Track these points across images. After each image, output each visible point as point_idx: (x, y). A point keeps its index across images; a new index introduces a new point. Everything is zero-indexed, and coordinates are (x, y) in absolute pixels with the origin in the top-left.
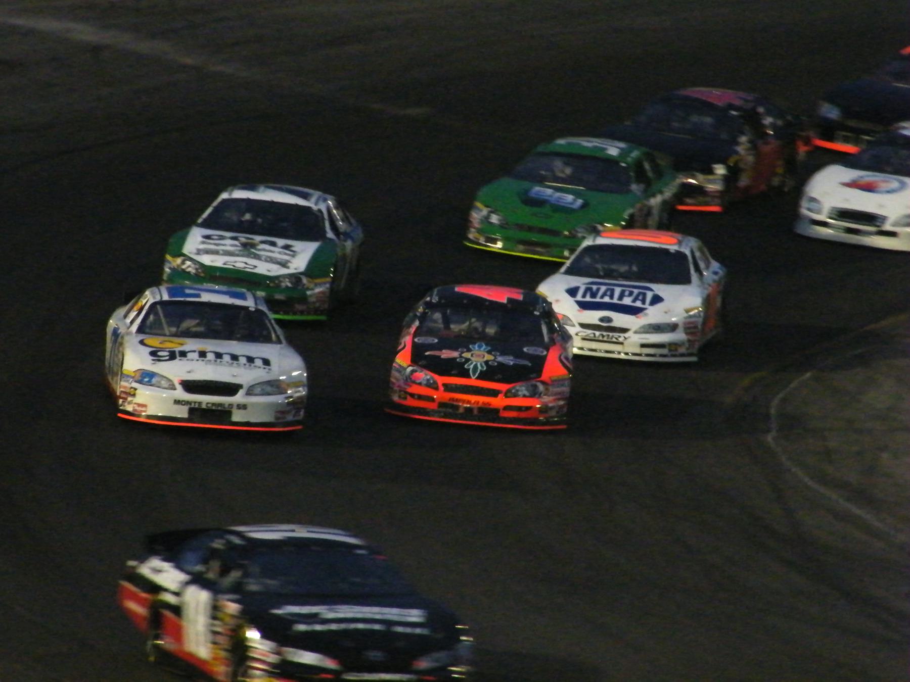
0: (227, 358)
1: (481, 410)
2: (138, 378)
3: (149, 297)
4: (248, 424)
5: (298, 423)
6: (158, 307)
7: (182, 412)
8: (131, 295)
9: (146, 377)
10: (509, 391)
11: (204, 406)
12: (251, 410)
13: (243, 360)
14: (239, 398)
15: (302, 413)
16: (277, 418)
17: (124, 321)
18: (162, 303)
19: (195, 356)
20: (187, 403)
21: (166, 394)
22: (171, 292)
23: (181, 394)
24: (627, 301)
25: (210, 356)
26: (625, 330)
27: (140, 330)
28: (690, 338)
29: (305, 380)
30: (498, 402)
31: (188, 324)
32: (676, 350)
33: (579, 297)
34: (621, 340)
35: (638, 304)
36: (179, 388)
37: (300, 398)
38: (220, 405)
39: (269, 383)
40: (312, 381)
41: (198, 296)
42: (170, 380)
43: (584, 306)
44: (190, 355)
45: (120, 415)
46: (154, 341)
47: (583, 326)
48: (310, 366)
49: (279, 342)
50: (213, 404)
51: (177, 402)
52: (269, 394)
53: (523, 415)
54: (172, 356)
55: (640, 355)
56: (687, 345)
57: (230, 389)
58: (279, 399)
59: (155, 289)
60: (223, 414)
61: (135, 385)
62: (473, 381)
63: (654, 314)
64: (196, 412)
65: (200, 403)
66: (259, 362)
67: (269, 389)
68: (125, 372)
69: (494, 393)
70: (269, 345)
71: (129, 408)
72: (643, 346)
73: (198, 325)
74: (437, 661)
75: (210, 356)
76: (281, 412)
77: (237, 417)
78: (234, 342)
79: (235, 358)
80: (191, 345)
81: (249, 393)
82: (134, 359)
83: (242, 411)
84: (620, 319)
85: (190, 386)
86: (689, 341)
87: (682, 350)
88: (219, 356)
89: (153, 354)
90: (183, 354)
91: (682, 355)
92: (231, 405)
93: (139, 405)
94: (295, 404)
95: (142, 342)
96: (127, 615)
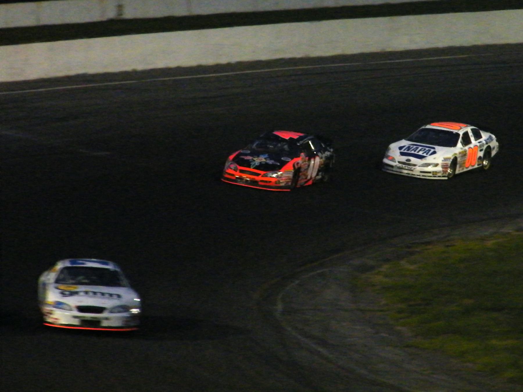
1: (251, 181)
3: (60, 266)
5: (135, 327)
7: (76, 322)
8: (50, 266)
9: (58, 305)
10: (264, 174)
12: (112, 320)
17: (49, 277)
21: (68, 313)
24: (421, 153)
26: (415, 165)
27: (57, 281)
28: (444, 169)
31: (81, 278)
32: (436, 174)
33: (402, 151)
34: (412, 169)
35: (425, 155)
38: (96, 318)
43: (402, 154)
46: (62, 287)
47: (399, 162)
48: (141, 295)
54: (72, 294)
55: (419, 175)
56: (442, 172)
57: (100, 310)
58: (125, 314)
60: (96, 322)
62: (251, 169)
63: (430, 159)
64: (85, 322)
67: (121, 310)
71: (49, 320)
72: (421, 172)
73: (84, 279)
77: (105, 324)
80: (81, 288)
81: (111, 312)
82: (52, 296)
84: (413, 160)
85: (81, 309)
86: (443, 171)
87: (439, 175)
90: (76, 293)
91: (439, 177)
94: (134, 316)
95: (57, 288)
96: (324, 168)
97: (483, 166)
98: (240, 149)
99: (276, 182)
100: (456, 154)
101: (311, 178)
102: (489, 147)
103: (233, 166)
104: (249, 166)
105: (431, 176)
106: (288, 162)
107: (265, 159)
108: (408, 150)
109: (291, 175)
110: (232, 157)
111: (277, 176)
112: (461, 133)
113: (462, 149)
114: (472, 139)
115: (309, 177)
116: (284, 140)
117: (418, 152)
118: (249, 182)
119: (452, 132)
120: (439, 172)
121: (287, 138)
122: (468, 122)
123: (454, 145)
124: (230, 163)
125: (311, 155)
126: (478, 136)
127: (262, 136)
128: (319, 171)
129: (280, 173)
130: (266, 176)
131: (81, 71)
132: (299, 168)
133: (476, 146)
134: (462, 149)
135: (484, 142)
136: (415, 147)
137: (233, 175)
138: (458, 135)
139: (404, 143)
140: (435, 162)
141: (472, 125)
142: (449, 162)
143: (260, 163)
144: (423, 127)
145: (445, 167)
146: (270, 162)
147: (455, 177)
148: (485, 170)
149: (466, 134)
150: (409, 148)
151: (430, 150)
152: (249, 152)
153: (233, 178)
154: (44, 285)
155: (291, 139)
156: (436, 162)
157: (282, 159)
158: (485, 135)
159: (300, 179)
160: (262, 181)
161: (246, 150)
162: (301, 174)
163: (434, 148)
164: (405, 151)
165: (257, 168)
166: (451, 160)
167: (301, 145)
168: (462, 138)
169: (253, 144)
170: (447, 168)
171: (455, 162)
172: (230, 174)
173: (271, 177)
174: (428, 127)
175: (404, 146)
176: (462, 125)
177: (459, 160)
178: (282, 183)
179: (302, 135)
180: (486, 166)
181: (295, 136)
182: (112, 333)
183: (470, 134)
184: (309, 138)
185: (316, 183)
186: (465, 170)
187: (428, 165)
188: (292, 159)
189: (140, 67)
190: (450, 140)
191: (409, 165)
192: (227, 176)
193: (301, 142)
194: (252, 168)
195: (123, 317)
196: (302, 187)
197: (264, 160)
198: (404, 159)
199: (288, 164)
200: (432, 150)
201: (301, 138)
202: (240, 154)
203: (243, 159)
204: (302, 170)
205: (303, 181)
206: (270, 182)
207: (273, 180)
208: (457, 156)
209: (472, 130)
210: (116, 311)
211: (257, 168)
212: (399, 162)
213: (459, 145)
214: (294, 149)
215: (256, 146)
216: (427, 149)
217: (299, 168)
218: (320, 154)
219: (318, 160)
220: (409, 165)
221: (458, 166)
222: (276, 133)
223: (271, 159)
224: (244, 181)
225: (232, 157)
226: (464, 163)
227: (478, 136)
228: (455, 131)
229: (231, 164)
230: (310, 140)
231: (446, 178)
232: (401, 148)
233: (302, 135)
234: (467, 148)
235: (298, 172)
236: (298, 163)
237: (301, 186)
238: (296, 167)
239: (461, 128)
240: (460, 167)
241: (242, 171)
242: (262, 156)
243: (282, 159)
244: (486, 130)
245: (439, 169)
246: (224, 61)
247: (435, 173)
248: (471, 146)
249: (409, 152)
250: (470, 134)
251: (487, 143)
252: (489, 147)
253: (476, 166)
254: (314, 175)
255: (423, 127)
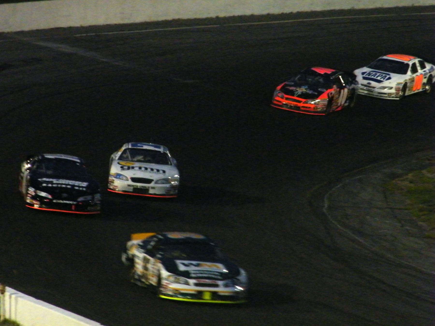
0: (149, 170)
1: (295, 107)
2: (115, 176)
4: (155, 194)
6: (128, 151)
7: (131, 189)
8: (117, 149)
9: (118, 176)
10: (305, 102)
11: (139, 187)
12: (156, 189)
13: (155, 171)
14: (152, 185)
15: (177, 191)
16: (166, 193)
18: (128, 149)
19: (137, 168)
20: (133, 186)
22: (132, 145)
23: (130, 182)
24: (379, 78)
25: (143, 169)
26: (374, 88)
27: (121, 158)
29: (178, 179)
30: (301, 105)
33: (364, 76)
35: (382, 79)
36: (130, 180)
37: (176, 185)
38: (145, 187)
39: (164, 179)
40: (182, 179)
41: (142, 147)
42: (126, 177)
43: (364, 78)
44: (135, 168)
45: (109, 190)
46: (123, 163)
48: (181, 174)
49: (171, 164)
50: (142, 187)
51: (129, 185)
52: (163, 183)
53: (305, 109)
54: (129, 168)
56: (395, 94)
57: (149, 181)
59: (127, 144)
60: (146, 190)
61: (114, 179)
62: (295, 98)
63: (386, 83)
64: (136, 190)
65: (137, 186)
66: (161, 172)
67: (164, 181)
68: (111, 174)
69: (300, 102)
70: (167, 166)
71: (111, 187)
74: (215, 282)
75: (143, 169)
76: (168, 190)
77: (151, 191)
78: (154, 164)
79: (152, 170)
80: (137, 165)
81: (156, 183)
82: (114, 169)
83: (153, 190)
84: (373, 84)
85: (134, 180)
86: (396, 93)
87: (393, 96)
88: (146, 169)
89: (122, 167)
90: (133, 168)
91: (393, 97)
92: (149, 187)
93: (115, 186)
94: (173, 187)
95: (119, 163)
97: (426, 90)
98: (285, 81)
99: (314, 108)
100: (406, 80)
101: (341, 105)
102: (431, 76)
103: (280, 95)
104: (293, 95)
105: (386, 97)
106: (324, 92)
107: (306, 89)
108: (369, 76)
109: (326, 103)
110: (279, 88)
111: (315, 103)
112: (411, 63)
113: (411, 76)
114: (419, 68)
115: (339, 104)
116: (320, 75)
117: (377, 77)
118: (293, 107)
119: (403, 63)
120: (393, 94)
121: (323, 74)
122: (416, 55)
123: (405, 72)
124: (277, 93)
125: (341, 87)
126: (423, 67)
127: (302, 71)
128: (347, 100)
129: (317, 101)
130: (307, 103)
131: (177, 17)
132: (333, 97)
133: (422, 74)
134: (411, 76)
135: (428, 71)
136: (374, 73)
137: (280, 102)
138: (408, 65)
139: (366, 69)
140: (391, 85)
141: (419, 57)
142: (401, 86)
143: (302, 92)
144: (380, 58)
145: (397, 90)
146: (310, 92)
147: (404, 97)
148: (427, 94)
149: (414, 65)
150: (369, 74)
151: (386, 76)
152: (293, 84)
153: (280, 104)
154: (112, 160)
155: (326, 74)
156: (391, 85)
157: (319, 89)
158: (428, 66)
159: (332, 106)
160: (302, 107)
161: (290, 82)
162: (333, 102)
163: (389, 75)
164: (367, 76)
165: (299, 96)
166: (403, 85)
167: (333, 79)
168: (412, 67)
169: (296, 77)
170: (399, 91)
171: (405, 86)
172: (278, 101)
173: (310, 104)
174: (385, 57)
175: (366, 72)
176: (412, 57)
177: (408, 84)
178: (319, 108)
179: (334, 71)
180: (428, 90)
181: (329, 71)
182: (156, 199)
183: (418, 65)
184: (341, 73)
185: (345, 109)
186: (413, 93)
187: (384, 88)
188: (327, 90)
189: (222, 15)
190: (401, 69)
191: (369, 87)
192: (275, 102)
193: (334, 77)
194: (295, 96)
195: (164, 188)
196: (334, 112)
197: (304, 90)
198: (366, 82)
199: (324, 94)
200: (388, 76)
201: (333, 74)
202: (286, 85)
203: (289, 89)
204: (335, 98)
205: (335, 107)
206: (310, 108)
207: (312, 106)
208: (407, 81)
209: (419, 61)
210: (160, 182)
211: (299, 96)
212: (362, 85)
213: (409, 73)
214: (329, 81)
215: (298, 79)
216: (384, 75)
217: (333, 97)
218: (348, 86)
219: (346, 90)
220: (369, 87)
221: (407, 89)
222: (313, 69)
223: (310, 90)
224: (289, 106)
225: (279, 88)
226: (412, 88)
227: (423, 67)
228: (406, 62)
229: (279, 93)
230: (340, 75)
231: (398, 99)
232: (363, 73)
233: (334, 71)
234: (414, 75)
235: (331, 100)
236: (331, 93)
237: (333, 111)
238: (330, 96)
239: (410, 60)
240: (409, 90)
241: (287, 99)
242: (303, 87)
243: (319, 89)
244: (429, 62)
245: (393, 91)
246: (287, 11)
247: (390, 94)
248: (418, 74)
249: (370, 77)
250: (418, 65)
251: (430, 72)
252: (431, 76)
253: (421, 90)
254: (343, 103)
255: (380, 58)
